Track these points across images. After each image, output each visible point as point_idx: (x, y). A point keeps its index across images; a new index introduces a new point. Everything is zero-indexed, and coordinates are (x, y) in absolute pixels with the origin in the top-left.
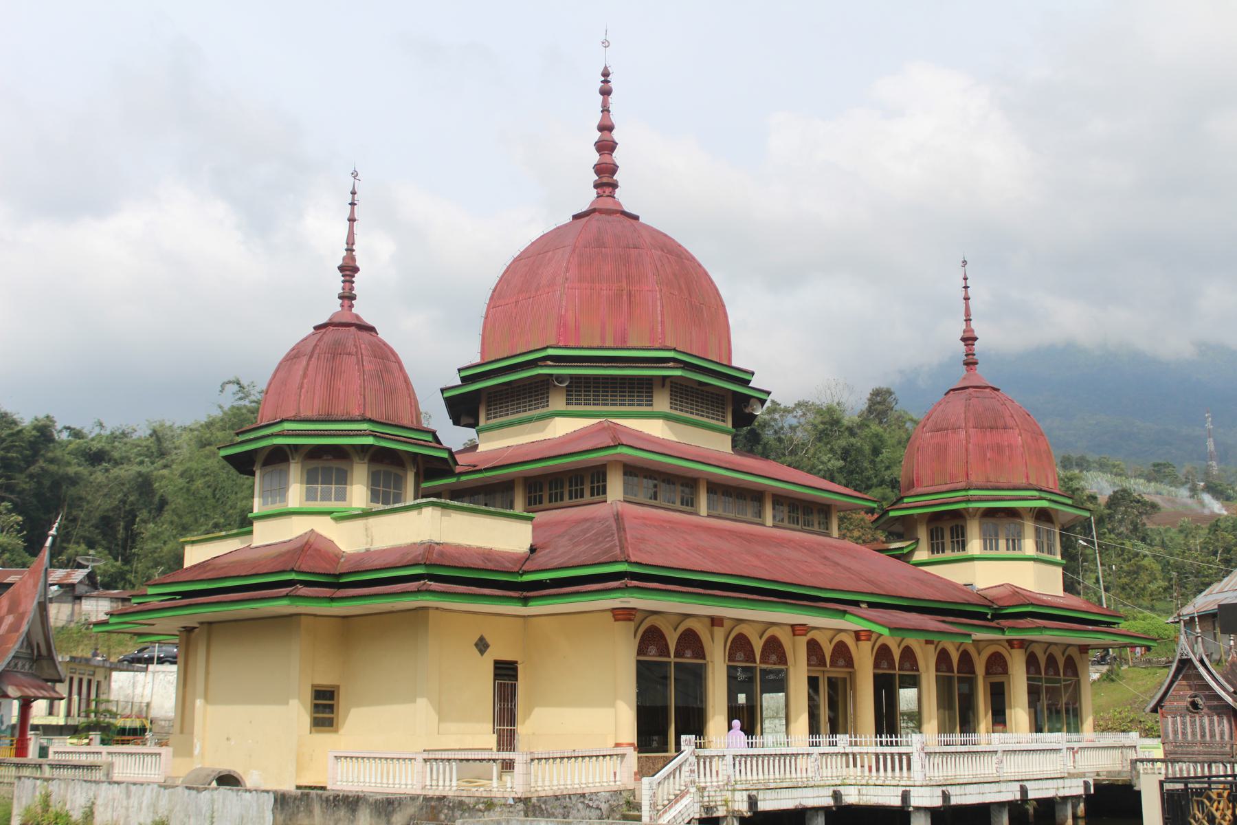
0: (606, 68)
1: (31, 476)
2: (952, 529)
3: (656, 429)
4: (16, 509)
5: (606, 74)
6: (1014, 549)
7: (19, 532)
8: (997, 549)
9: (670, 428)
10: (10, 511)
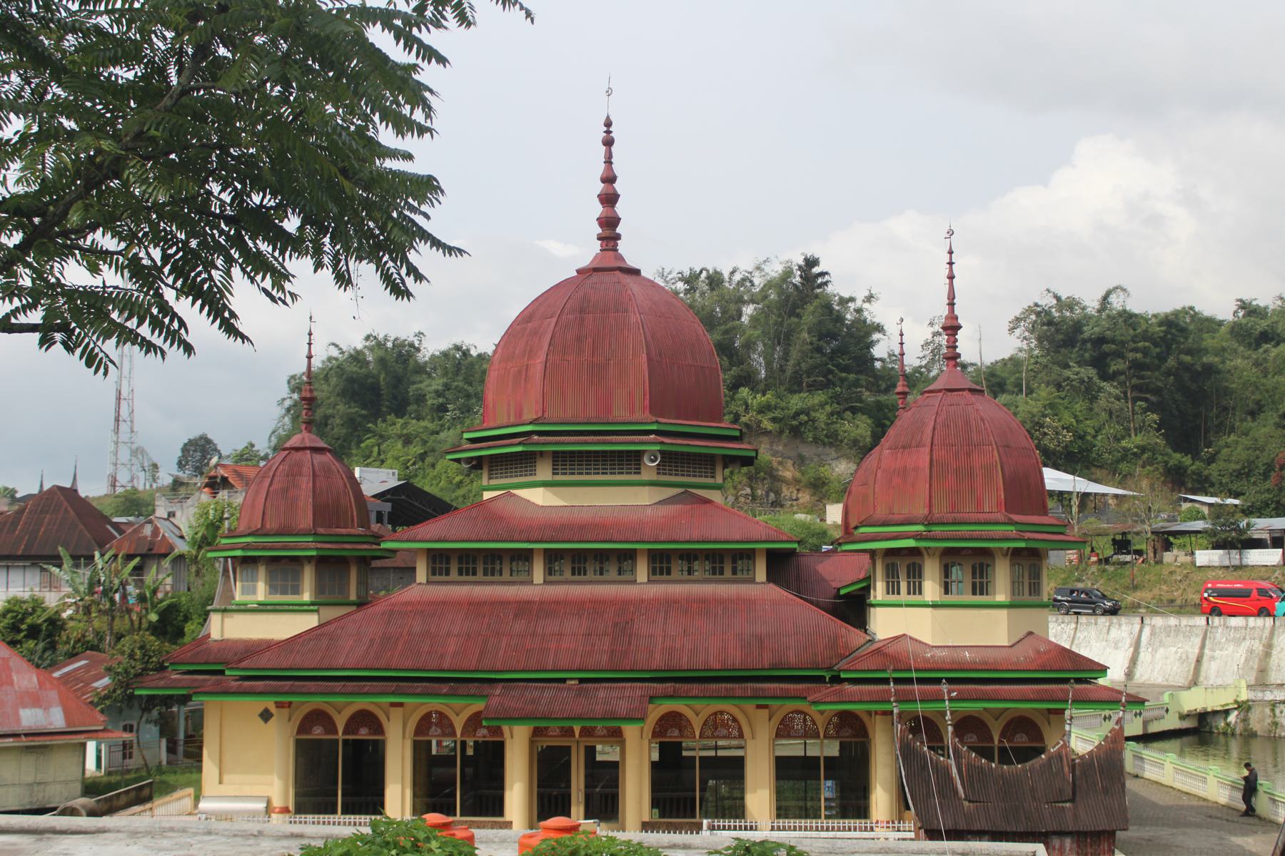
0: (608, 117)
1: (1169, 373)
2: (908, 567)
3: (538, 497)
4: (1152, 408)
5: (608, 124)
6: (982, 594)
7: (1158, 430)
8: (899, 593)
9: (555, 494)
10: (1145, 411)
